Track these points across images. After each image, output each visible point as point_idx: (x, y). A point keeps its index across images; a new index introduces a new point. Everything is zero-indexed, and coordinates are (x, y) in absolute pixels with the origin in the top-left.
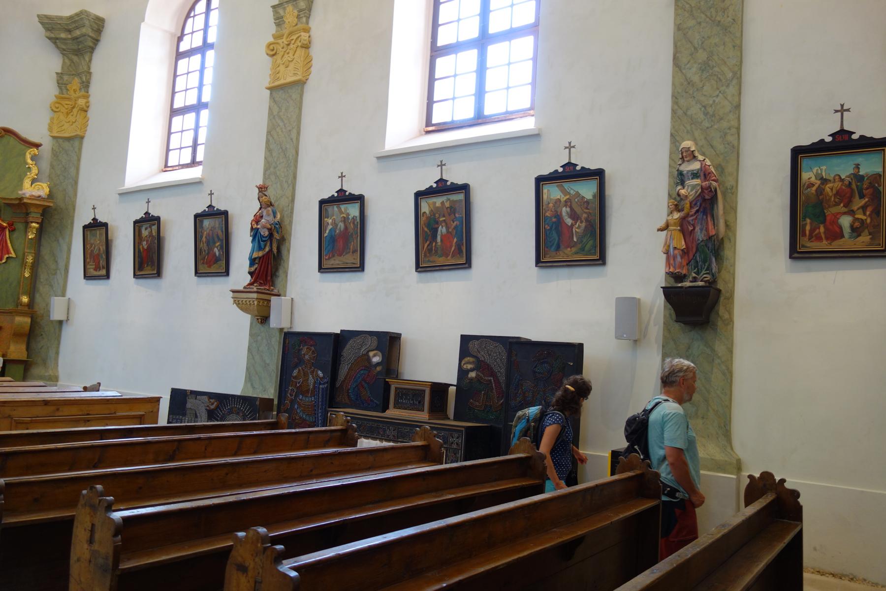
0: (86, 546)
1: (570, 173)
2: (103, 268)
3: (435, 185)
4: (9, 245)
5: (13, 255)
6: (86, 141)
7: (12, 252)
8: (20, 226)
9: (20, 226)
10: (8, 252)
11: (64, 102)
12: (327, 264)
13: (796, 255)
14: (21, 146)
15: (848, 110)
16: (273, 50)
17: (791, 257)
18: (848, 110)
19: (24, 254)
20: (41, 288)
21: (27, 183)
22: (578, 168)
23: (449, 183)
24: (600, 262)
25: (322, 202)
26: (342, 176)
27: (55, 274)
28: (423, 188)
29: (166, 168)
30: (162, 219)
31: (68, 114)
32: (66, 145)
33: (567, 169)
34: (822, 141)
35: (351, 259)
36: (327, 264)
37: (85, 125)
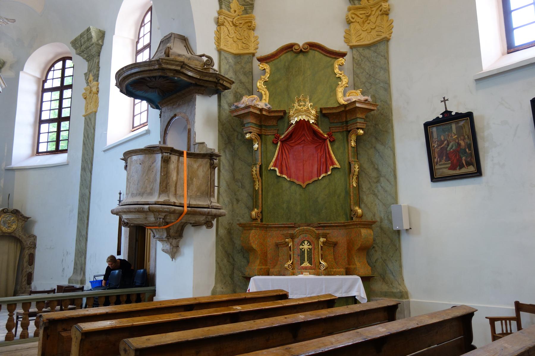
0: (73, 336)
1: (448, 117)
2: (469, 164)
3: (441, 116)
4: (333, 155)
5: (338, 165)
6: (393, 45)
7: (337, 162)
8: (338, 136)
9: (338, 136)
10: (333, 163)
11: (358, 13)
12: (438, 175)
13: (434, 180)
14: (326, 59)
15: (447, 100)
16: (353, 18)
17: (432, 181)
18: (447, 100)
19: (350, 164)
20: (365, 197)
21: (340, 91)
22: (453, 114)
23: (453, 114)
24: (478, 174)
25: (427, 125)
26: (444, 100)
27: (378, 181)
28: (431, 119)
29: (511, 48)
30: (474, 115)
31: (364, 23)
32: (367, 52)
33: (446, 115)
34: (438, 117)
35: (443, 170)
36: (438, 175)
37: (390, 27)
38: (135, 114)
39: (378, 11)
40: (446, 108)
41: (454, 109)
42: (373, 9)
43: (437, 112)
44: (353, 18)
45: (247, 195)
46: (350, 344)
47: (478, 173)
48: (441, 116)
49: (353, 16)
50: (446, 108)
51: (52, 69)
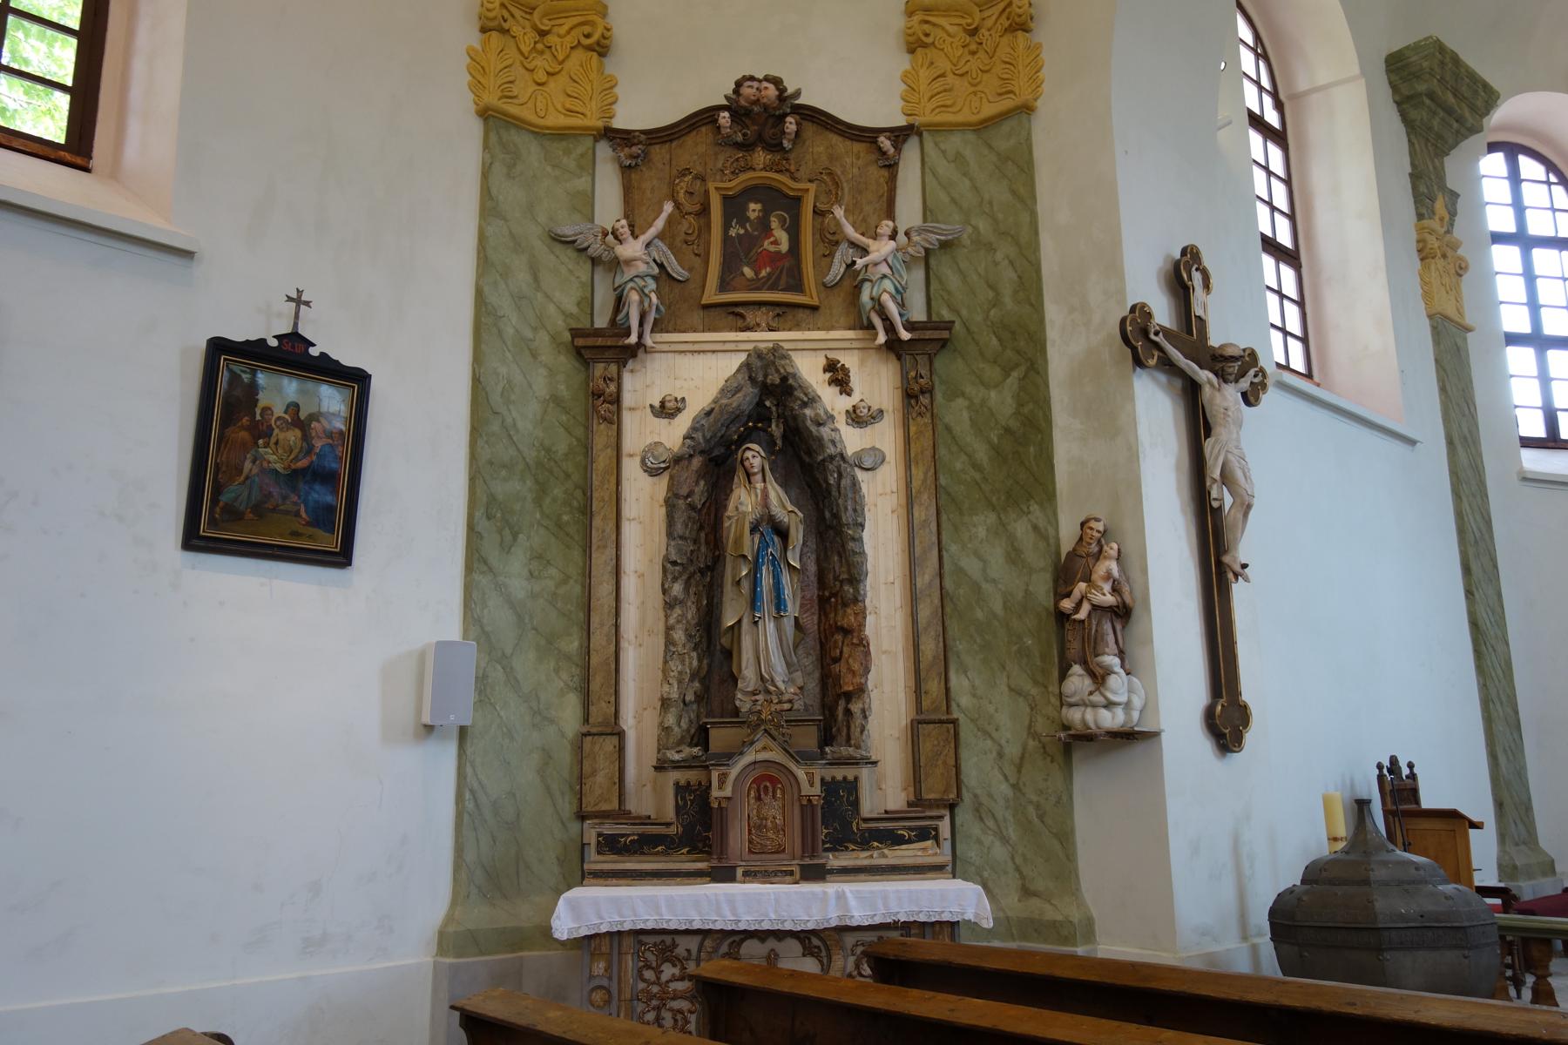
3: (274, 343)
24: (340, 559)
28: (238, 336)
30: (375, 384)
33: (288, 347)
38: (1286, 302)
39: (1003, 20)
40: (296, 325)
41: (327, 341)
42: (986, 14)
43: (266, 327)
44: (927, 35)
45: (324, 409)
46: (1093, 978)
47: (342, 557)
48: (274, 343)
49: (926, 27)
50: (296, 325)
51: (1553, 179)
